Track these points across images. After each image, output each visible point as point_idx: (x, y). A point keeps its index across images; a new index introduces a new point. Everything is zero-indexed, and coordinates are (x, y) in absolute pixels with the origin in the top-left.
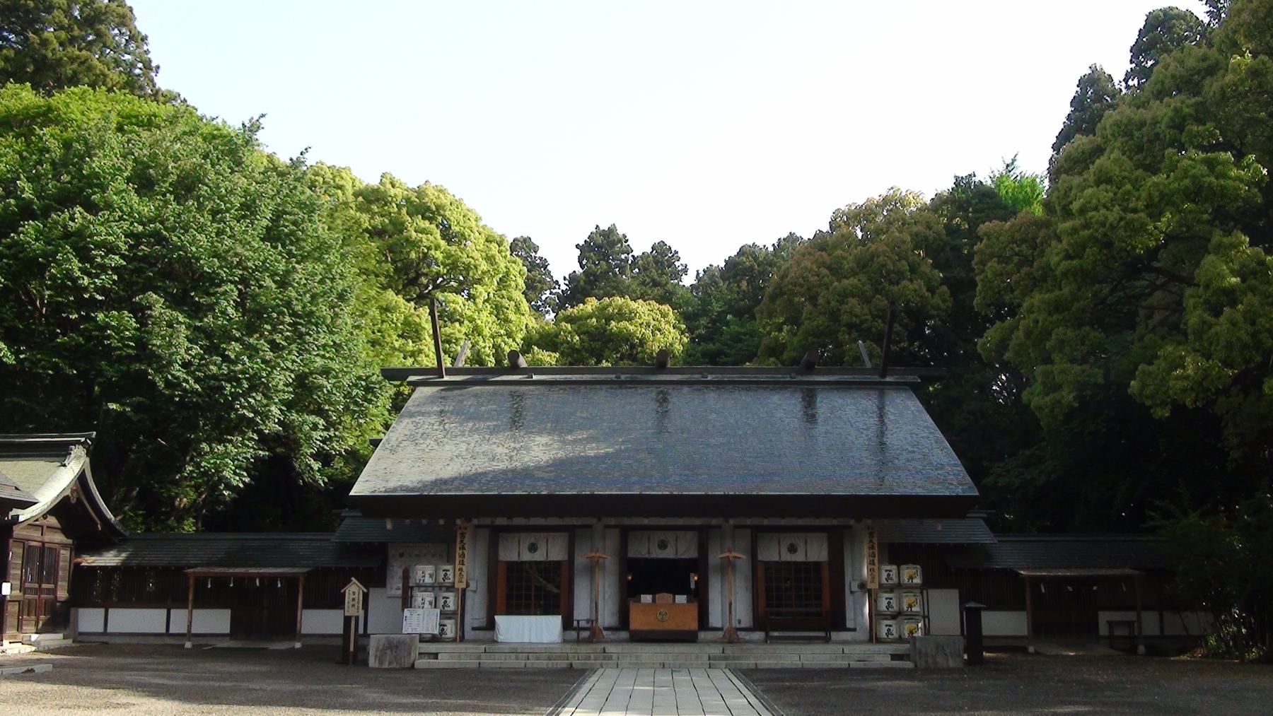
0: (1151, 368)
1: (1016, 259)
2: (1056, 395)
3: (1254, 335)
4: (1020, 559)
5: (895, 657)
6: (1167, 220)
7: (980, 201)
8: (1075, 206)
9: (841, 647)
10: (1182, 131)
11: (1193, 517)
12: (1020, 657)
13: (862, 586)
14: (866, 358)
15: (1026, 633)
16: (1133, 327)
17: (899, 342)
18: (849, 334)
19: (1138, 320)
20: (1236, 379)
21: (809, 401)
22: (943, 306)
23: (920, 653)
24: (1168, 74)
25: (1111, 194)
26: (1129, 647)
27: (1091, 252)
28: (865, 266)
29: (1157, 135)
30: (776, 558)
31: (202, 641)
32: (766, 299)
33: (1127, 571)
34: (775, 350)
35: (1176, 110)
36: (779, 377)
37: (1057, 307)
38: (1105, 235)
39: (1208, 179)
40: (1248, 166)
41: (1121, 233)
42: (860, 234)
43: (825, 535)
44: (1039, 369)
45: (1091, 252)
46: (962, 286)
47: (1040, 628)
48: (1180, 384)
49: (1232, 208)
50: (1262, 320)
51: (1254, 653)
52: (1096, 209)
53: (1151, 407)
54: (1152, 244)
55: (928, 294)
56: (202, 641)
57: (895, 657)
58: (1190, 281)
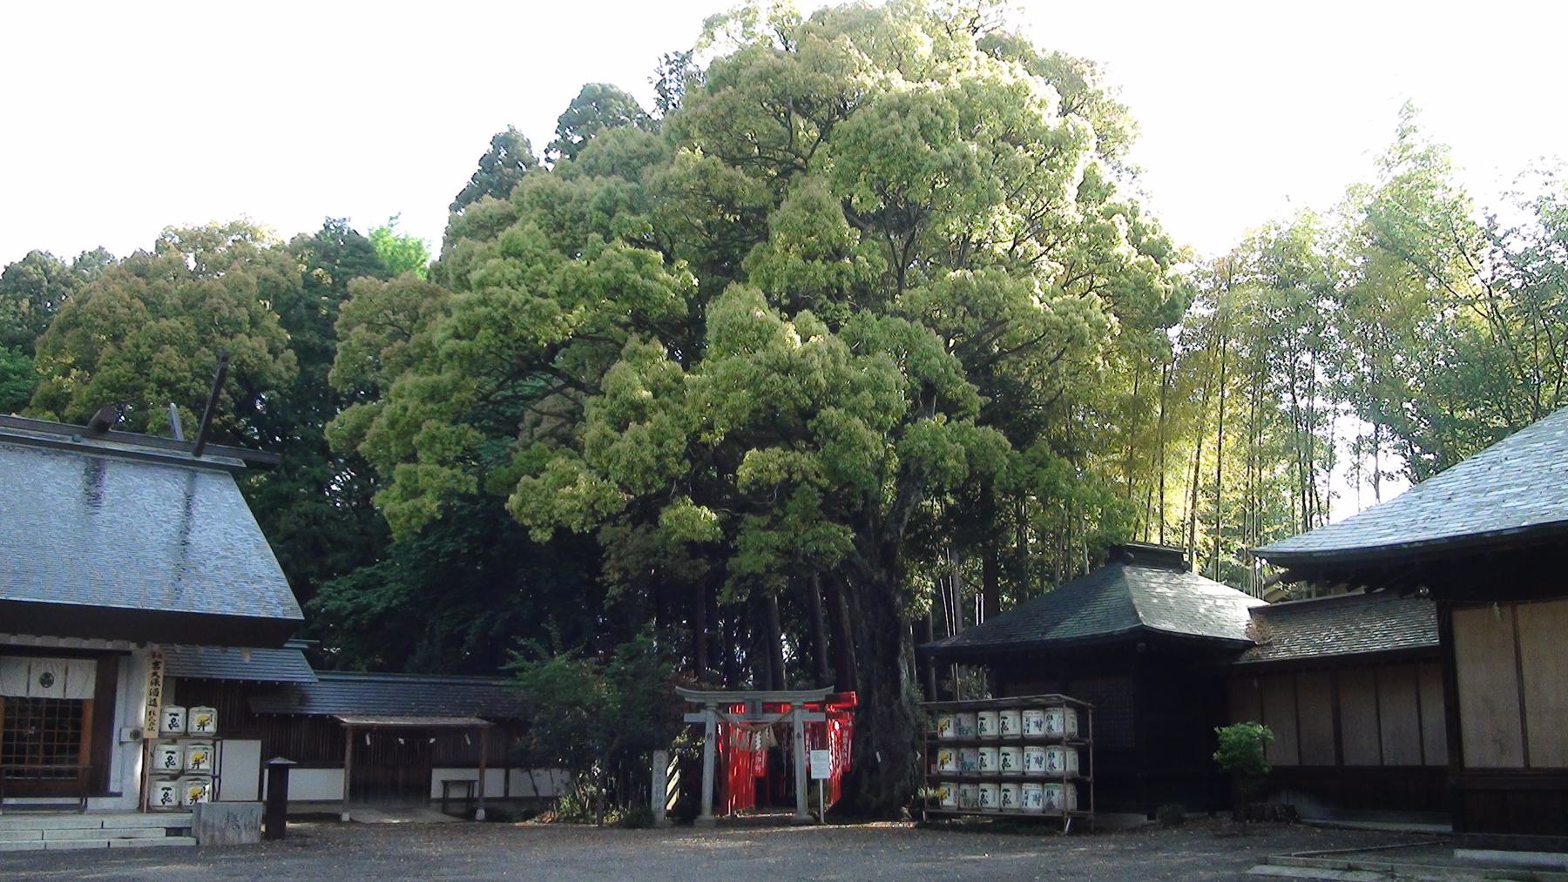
0: (536, 482)
1: (389, 329)
2: (417, 502)
3: (658, 458)
4: (343, 701)
5: (170, 831)
6: (579, 315)
7: (352, 253)
8: (475, 276)
9: (99, 819)
10: (611, 216)
11: (560, 660)
12: (330, 827)
13: (136, 734)
14: (177, 426)
15: (341, 797)
16: (515, 434)
17: (222, 414)
18: (159, 393)
19: (521, 426)
20: (630, 506)
21: (94, 476)
22: (286, 376)
23: (205, 825)
24: (605, 150)
25: (519, 271)
26: (467, 811)
27: (485, 335)
28: (192, 306)
29: (583, 215)
30: (22, 693)
31: (492, 804)
32: (53, 328)
33: (474, 721)
34: (55, 402)
35: (609, 192)
36: (56, 437)
37: (434, 394)
38: (505, 317)
39: (632, 276)
40: (680, 271)
41: (525, 318)
42: (192, 265)
43: (94, 662)
44: (401, 467)
45: (485, 335)
46: (314, 355)
47: (359, 791)
48: (567, 505)
49: (656, 313)
50: (670, 443)
51: (615, 816)
52: (498, 284)
53: (529, 528)
54: (559, 337)
55: (270, 357)
56: (492, 804)
57: (170, 831)
58: (596, 391)
